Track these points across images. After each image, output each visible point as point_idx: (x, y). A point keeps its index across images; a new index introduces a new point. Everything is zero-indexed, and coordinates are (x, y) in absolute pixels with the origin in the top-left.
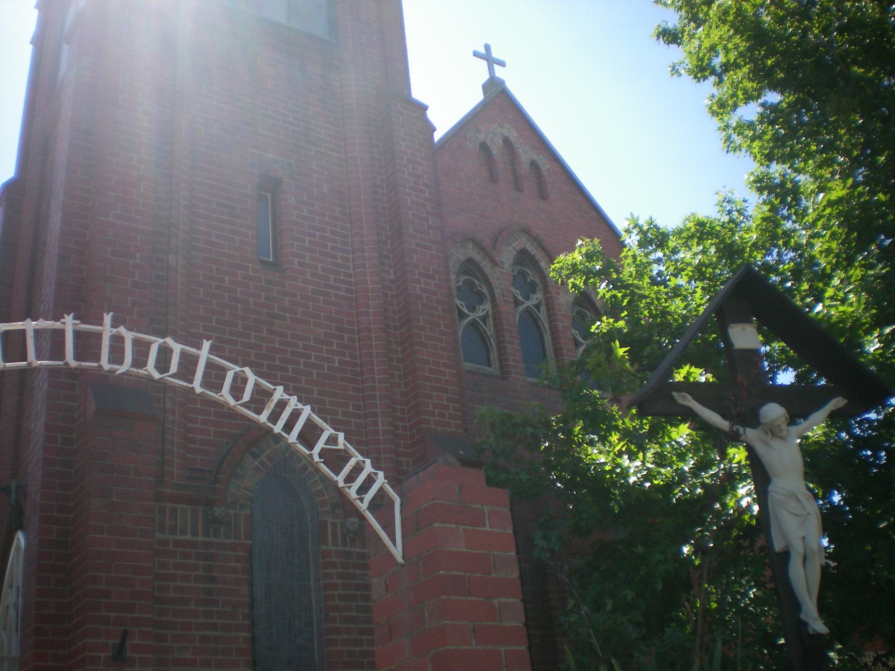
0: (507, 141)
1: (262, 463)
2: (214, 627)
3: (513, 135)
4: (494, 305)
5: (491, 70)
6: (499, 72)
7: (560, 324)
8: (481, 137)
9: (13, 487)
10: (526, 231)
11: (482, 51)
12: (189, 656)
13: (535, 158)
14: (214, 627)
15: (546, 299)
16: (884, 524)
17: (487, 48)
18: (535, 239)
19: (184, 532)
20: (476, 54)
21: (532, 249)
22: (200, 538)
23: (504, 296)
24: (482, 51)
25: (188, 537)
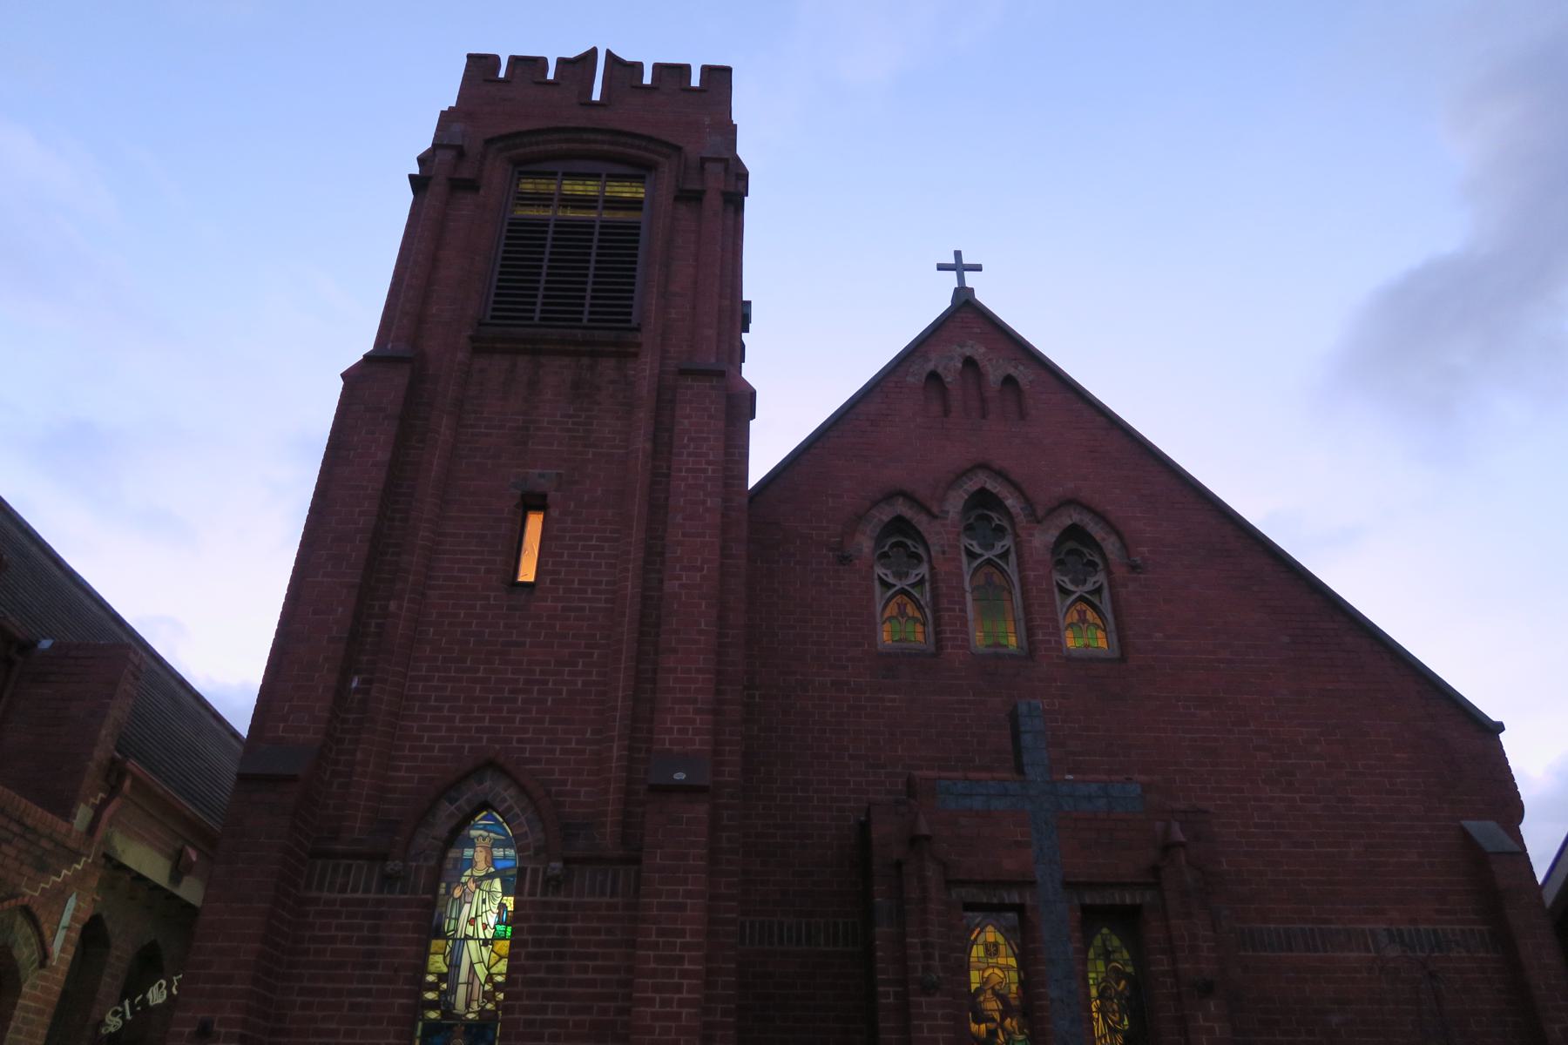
0: (969, 362)
1: (458, 808)
2: (368, 993)
3: (978, 351)
4: (932, 568)
5: (961, 279)
6: (971, 279)
7: (1032, 574)
8: (930, 366)
9: (1143, 778)
10: (984, 466)
11: (952, 261)
12: (333, 1026)
13: (1011, 371)
14: (368, 993)
15: (1016, 544)
16: (482, 913)
17: (958, 254)
18: (1001, 475)
19: (354, 890)
20: (941, 267)
21: (993, 486)
22: (371, 896)
23: (944, 553)
24: (952, 261)
25: (359, 895)
